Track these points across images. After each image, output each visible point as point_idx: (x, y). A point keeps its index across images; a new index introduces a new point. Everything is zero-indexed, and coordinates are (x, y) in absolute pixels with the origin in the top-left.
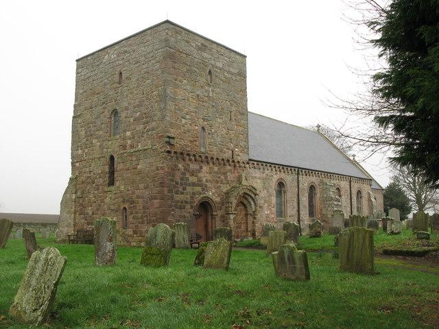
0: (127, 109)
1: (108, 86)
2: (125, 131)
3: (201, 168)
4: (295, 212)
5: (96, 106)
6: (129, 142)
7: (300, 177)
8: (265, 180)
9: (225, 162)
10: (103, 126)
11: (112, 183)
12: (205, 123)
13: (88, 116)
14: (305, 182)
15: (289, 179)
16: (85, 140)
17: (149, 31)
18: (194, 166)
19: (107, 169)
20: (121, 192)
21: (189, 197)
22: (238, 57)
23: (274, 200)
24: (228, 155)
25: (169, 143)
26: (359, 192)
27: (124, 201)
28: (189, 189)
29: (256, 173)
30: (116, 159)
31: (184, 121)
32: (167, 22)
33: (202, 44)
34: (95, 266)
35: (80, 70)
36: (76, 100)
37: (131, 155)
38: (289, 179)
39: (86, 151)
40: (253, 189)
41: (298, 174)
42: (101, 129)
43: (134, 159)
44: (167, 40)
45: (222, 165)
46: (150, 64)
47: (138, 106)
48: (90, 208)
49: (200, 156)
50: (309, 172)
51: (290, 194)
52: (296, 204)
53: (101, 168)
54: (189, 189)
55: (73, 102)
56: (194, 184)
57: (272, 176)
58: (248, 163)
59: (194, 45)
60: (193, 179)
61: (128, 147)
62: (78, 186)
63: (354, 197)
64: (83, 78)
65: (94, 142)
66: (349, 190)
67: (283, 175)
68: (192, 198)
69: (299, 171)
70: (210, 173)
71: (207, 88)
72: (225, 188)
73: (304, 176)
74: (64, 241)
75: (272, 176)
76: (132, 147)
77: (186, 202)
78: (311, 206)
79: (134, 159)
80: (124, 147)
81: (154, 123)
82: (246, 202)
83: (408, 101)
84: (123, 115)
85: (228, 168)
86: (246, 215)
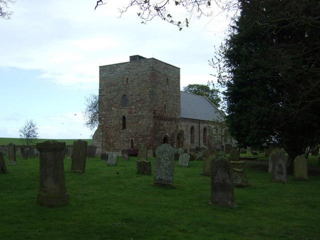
0: (132, 95)
1: (120, 83)
4: (198, 142)
6: (134, 111)
11: (124, 127)
14: (202, 126)
15: (195, 125)
18: (162, 122)
19: (121, 122)
20: (130, 133)
23: (189, 135)
24: (173, 116)
25: (155, 113)
28: (160, 132)
29: (183, 124)
32: (153, 59)
35: (102, 72)
38: (195, 125)
39: (108, 112)
40: (182, 131)
44: (152, 67)
47: (138, 95)
50: (204, 122)
51: (196, 133)
52: (198, 138)
53: (117, 122)
54: (160, 132)
60: (162, 128)
67: (193, 124)
68: (162, 136)
69: (199, 121)
72: (172, 131)
74: (229, 173)
76: (135, 113)
78: (204, 138)
80: (131, 113)
83: (235, 81)
85: (174, 122)
86: (179, 143)
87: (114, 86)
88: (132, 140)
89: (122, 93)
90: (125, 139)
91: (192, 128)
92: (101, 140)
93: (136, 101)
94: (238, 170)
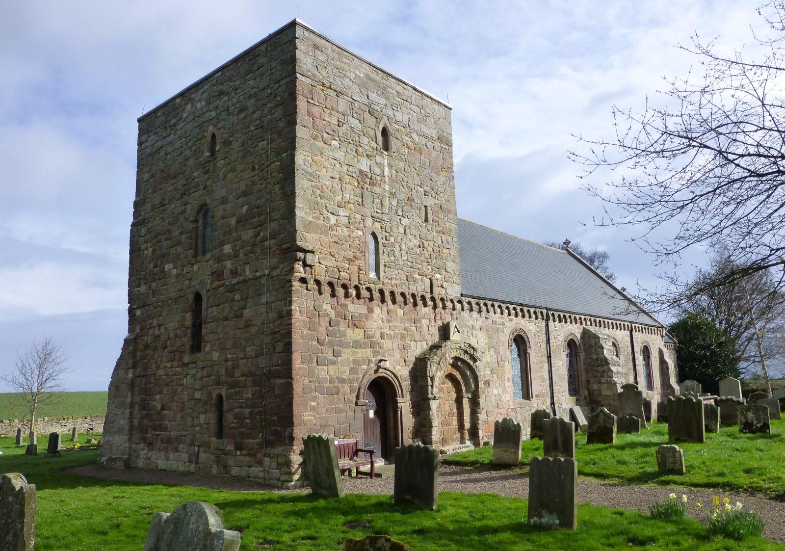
0: (224, 201)
1: (191, 162)
2: (222, 244)
3: (371, 310)
5: (170, 202)
7: (551, 323)
8: (491, 332)
9: (417, 300)
10: (184, 236)
11: (196, 347)
12: (378, 225)
13: (158, 221)
14: (562, 332)
15: (532, 328)
16: (152, 266)
17: (263, 48)
18: (355, 308)
21: (347, 369)
22: (436, 107)
24: (421, 287)
26: (646, 351)
27: (218, 383)
30: (205, 299)
31: (333, 220)
33: (367, 76)
34: (360, 314)
35: (144, 138)
36: (138, 194)
37: (232, 289)
38: (532, 328)
39: (154, 285)
41: (547, 320)
42: (179, 243)
43: (237, 297)
45: (411, 305)
46: (266, 111)
47: (245, 194)
48: (158, 396)
49: (369, 289)
51: (536, 354)
55: (133, 198)
56: (356, 344)
57: (503, 324)
58: (460, 302)
59: (353, 77)
61: (227, 273)
62: (139, 354)
63: (640, 358)
64: (148, 151)
65: (167, 267)
66: (630, 345)
70: (389, 321)
71: (378, 159)
73: (557, 323)
75: (503, 324)
76: (234, 273)
77: (342, 381)
79: (237, 297)
81: (274, 225)
82: (457, 375)
84: (219, 212)
87: (175, 177)
88: (220, 397)
89: (194, 201)
90: (198, 395)
91: (520, 342)
92: (129, 400)
93: (238, 222)
94: (259, 409)
